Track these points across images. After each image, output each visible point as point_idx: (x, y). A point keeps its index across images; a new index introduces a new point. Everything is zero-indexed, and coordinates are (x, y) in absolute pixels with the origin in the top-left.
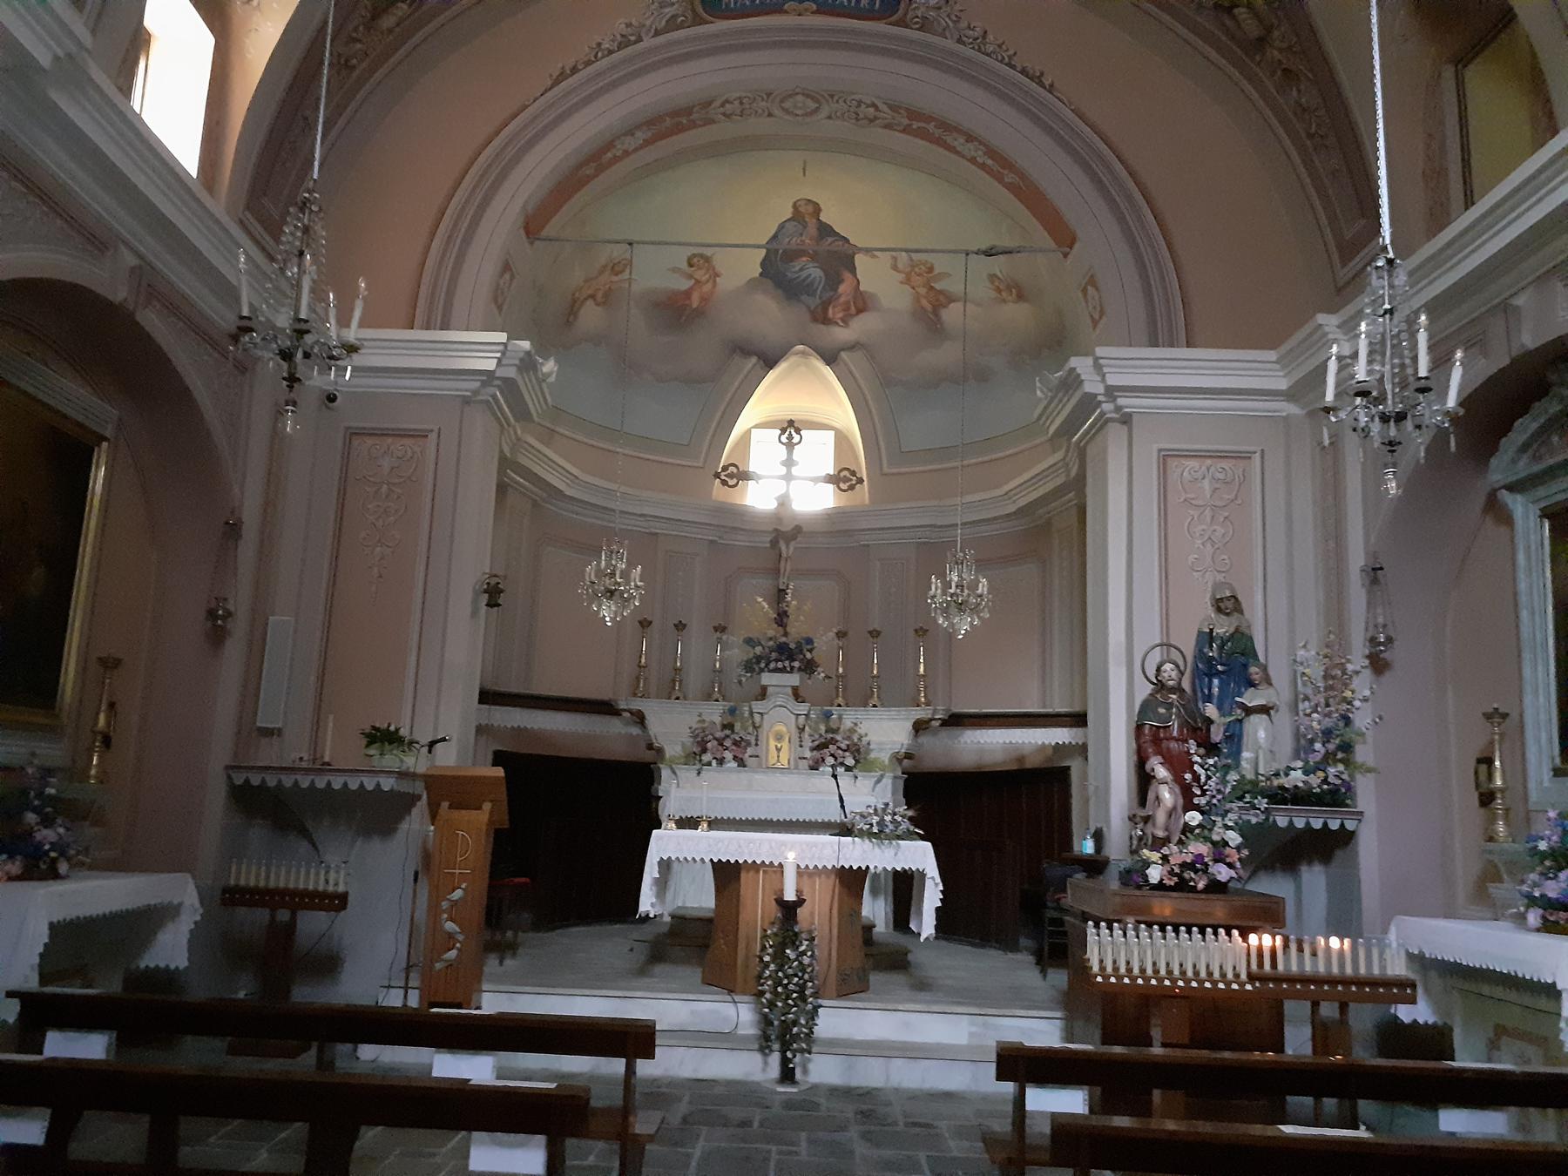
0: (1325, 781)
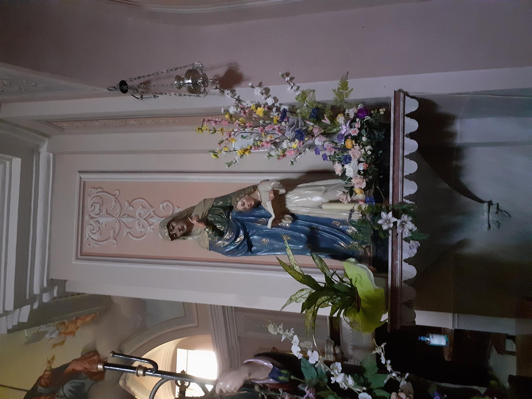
0: (357, 139)
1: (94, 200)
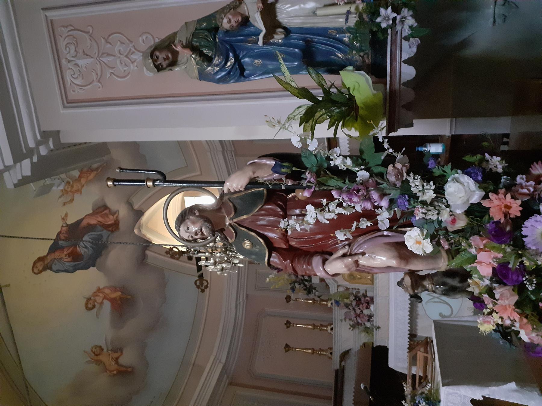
1: (67, 40)
